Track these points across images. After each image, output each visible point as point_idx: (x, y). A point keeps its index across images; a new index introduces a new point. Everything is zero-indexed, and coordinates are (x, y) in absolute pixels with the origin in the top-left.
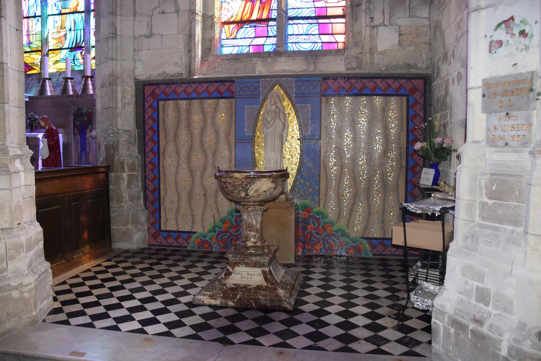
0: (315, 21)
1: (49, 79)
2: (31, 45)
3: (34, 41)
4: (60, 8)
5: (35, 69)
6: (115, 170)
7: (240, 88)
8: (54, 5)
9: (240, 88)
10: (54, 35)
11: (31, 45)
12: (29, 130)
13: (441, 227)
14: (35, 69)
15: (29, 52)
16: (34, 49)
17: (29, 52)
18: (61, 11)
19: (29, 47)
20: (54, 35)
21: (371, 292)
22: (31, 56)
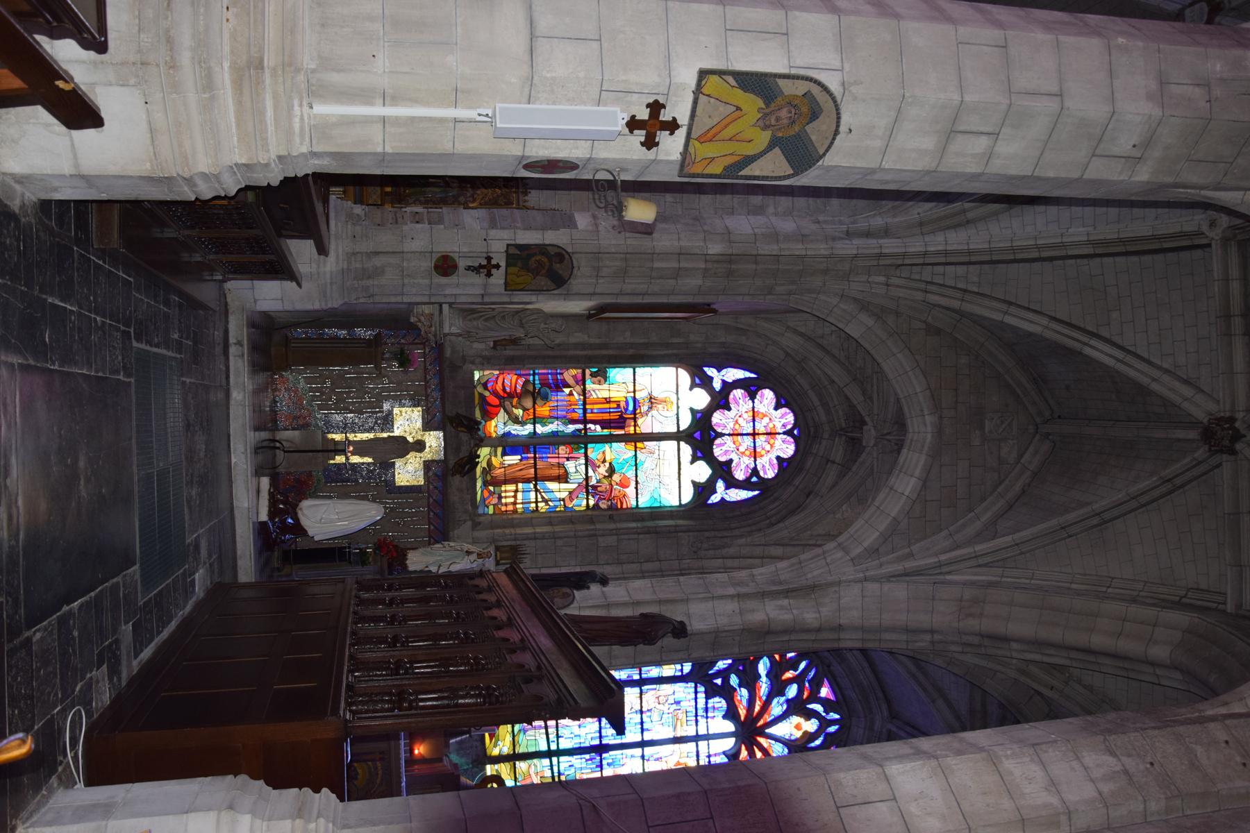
0: (626, 575)
1: (470, 736)
2: (522, 733)
3: (528, 738)
4: (566, 773)
5: (491, 742)
6: (257, 525)
7: (785, 34)
8: (570, 764)
9: (785, 34)
10: (533, 767)
11: (522, 733)
12: (513, 251)
13: (382, 127)
14: (491, 742)
15: (513, 731)
16: (516, 738)
17: (513, 731)
18: (563, 774)
19: (520, 731)
20: (533, 767)
21: (767, 676)
22: (508, 735)
